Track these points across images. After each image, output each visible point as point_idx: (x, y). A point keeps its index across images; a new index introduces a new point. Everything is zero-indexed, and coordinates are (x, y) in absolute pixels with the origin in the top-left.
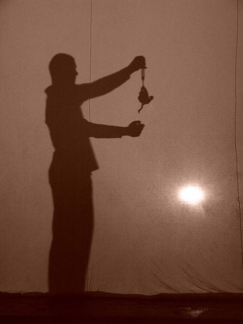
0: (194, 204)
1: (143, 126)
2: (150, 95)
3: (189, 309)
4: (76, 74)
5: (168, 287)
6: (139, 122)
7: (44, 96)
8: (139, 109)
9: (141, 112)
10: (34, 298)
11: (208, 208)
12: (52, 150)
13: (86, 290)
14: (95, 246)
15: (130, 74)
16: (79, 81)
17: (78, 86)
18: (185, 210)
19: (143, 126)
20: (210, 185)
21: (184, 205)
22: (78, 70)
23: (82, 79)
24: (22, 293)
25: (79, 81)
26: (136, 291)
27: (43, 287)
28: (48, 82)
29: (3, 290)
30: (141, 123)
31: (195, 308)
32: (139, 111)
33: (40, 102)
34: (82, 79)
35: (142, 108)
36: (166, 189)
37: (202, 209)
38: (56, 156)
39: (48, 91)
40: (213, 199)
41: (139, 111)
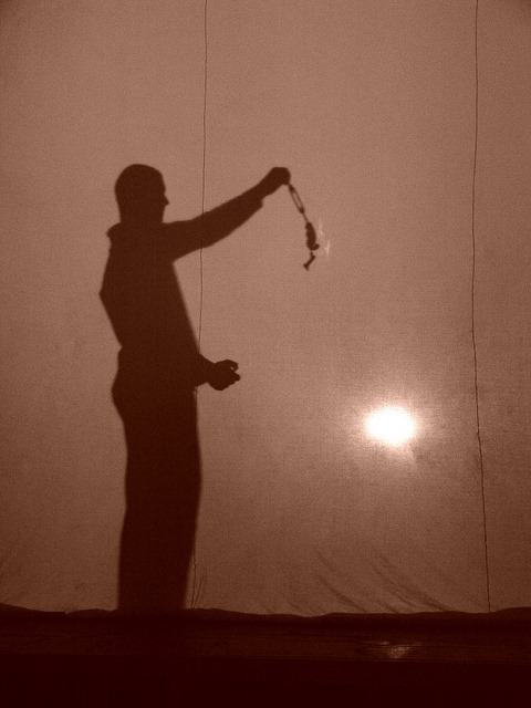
0: (394, 445)
2: (317, 242)
3: (385, 643)
5: (344, 599)
6: (235, 365)
7: (104, 245)
8: (306, 261)
9: (311, 266)
10: (93, 619)
11: (423, 452)
12: (117, 347)
14: (204, 520)
15: (262, 197)
16: (171, 215)
18: (378, 456)
19: (237, 378)
22: (169, 194)
23: (180, 207)
25: (171, 215)
26: (284, 609)
27: (110, 604)
28: (113, 217)
30: (238, 372)
31: (394, 643)
32: (306, 266)
33: (97, 253)
34: (180, 207)
35: (313, 257)
36: (343, 417)
37: (410, 454)
39: (113, 233)
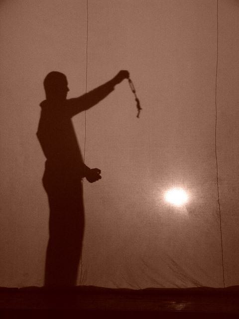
1: (100, 177)
4: (68, 90)
6: (100, 171)
7: (39, 109)
8: (137, 115)
11: (192, 209)
12: (43, 159)
13: (78, 284)
16: (70, 96)
17: (68, 100)
18: (170, 211)
19: (100, 177)
20: (193, 189)
21: (169, 207)
22: (69, 86)
23: (75, 91)
24: (19, 288)
25: (70, 96)
26: (125, 286)
27: (41, 284)
28: (43, 97)
29: (1, 286)
30: (100, 175)
31: (178, 303)
32: (138, 116)
33: (34, 116)
34: (75, 91)
36: (154, 193)
38: (47, 164)
39: (42, 105)
40: (195, 202)
41: (138, 116)
